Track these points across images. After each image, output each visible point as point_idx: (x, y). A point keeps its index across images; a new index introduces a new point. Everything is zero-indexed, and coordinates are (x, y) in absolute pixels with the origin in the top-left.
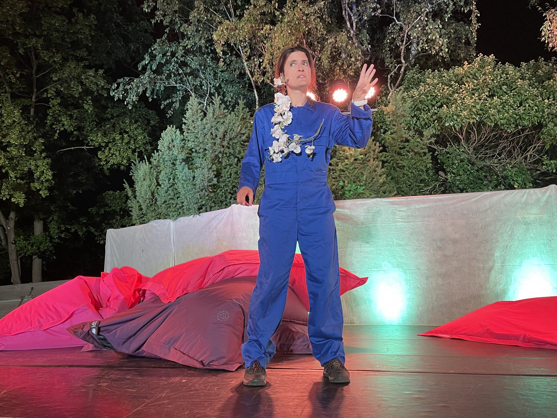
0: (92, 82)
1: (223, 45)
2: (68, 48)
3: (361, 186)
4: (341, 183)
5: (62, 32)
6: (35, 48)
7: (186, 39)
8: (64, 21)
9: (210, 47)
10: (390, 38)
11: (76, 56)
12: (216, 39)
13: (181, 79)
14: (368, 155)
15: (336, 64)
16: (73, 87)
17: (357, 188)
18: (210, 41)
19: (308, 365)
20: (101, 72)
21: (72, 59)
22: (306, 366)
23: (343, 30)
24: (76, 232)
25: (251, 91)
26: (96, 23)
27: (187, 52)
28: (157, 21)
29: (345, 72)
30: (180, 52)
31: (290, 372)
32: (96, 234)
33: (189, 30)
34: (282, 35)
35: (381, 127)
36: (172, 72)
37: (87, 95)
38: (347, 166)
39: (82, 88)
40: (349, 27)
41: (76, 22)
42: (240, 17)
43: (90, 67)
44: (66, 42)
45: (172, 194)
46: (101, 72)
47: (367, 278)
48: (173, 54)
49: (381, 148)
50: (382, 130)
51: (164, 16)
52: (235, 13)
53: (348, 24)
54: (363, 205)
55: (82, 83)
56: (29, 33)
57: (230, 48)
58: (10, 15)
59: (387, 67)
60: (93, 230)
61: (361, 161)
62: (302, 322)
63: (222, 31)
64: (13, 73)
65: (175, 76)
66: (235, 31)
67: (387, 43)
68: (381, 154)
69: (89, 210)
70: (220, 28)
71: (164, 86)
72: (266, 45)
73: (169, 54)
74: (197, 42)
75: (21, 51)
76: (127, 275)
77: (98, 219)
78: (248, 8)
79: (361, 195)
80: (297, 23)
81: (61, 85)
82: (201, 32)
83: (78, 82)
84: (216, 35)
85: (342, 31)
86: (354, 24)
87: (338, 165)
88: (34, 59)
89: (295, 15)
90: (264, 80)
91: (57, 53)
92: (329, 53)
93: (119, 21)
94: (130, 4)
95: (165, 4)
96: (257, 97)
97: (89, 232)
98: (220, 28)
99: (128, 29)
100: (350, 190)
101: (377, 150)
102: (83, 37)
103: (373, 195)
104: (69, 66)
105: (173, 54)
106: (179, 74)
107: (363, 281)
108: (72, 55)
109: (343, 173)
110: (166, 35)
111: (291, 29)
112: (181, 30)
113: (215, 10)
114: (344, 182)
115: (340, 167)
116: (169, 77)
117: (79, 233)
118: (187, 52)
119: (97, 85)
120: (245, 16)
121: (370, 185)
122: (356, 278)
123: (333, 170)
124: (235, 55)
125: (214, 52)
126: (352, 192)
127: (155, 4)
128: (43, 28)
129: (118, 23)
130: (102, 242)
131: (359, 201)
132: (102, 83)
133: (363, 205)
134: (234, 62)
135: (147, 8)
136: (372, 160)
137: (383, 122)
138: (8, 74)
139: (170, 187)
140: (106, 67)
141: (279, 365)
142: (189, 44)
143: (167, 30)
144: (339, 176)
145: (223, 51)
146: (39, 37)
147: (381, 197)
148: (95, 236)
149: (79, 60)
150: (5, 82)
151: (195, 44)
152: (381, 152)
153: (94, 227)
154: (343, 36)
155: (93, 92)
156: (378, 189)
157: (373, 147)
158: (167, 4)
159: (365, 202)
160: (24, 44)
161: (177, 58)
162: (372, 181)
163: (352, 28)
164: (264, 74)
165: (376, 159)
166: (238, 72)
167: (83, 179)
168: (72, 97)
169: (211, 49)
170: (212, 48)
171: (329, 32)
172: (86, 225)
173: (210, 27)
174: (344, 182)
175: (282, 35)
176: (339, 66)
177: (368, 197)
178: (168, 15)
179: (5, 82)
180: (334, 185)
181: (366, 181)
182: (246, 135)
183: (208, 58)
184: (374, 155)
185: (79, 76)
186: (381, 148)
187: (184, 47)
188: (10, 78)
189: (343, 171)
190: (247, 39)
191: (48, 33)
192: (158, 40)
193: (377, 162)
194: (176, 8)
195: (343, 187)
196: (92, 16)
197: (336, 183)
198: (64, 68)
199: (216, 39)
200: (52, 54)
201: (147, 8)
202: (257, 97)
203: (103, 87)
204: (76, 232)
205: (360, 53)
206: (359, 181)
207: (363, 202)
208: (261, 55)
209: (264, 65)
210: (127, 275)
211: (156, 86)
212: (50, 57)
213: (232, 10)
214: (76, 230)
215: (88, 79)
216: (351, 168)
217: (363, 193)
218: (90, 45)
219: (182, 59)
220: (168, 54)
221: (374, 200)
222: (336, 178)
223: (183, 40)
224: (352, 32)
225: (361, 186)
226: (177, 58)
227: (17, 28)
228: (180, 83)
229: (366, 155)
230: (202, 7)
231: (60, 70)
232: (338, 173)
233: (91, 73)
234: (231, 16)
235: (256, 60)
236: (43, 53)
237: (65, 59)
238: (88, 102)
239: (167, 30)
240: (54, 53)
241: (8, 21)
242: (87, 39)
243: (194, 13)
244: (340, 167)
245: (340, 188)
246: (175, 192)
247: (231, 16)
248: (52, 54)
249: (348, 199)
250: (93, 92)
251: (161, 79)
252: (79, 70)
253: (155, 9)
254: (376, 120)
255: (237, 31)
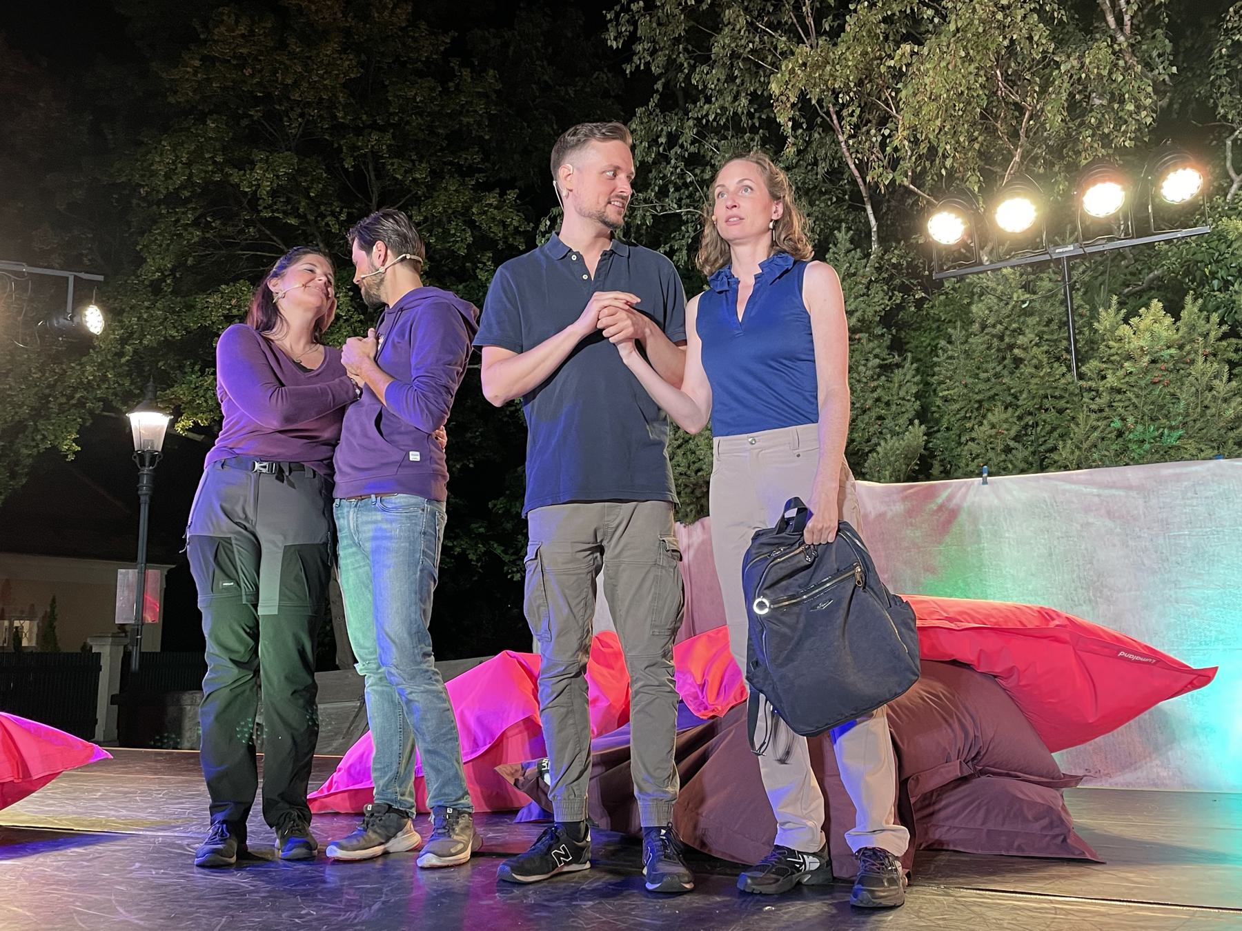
0: (494, 219)
1: (793, 105)
2: (442, 150)
3: (1171, 428)
4: (1117, 424)
5: (429, 114)
6: (375, 155)
7: (703, 100)
8: (432, 89)
9: (757, 115)
10: (1229, 42)
11: (459, 166)
12: (777, 92)
13: (690, 196)
14: (1188, 347)
15: (1082, 124)
16: (454, 235)
17: (1162, 434)
18: (762, 101)
19: (1075, 888)
20: (512, 195)
21: (449, 172)
22: (1075, 888)
23: (1098, 36)
24: (464, 554)
25: (856, 209)
26: (499, 86)
27: (704, 129)
28: (638, 67)
29: (1106, 140)
30: (690, 133)
31: (1031, 902)
32: (506, 558)
33: (712, 77)
34: (943, 64)
35: (1213, 275)
36: (671, 182)
37: (484, 250)
38: (1132, 379)
39: (473, 235)
40: (1113, 26)
41: (458, 89)
42: (835, 33)
43: (486, 187)
44: (438, 135)
45: (684, 462)
46: (512, 195)
47: (1216, 669)
48: (673, 139)
49: (1225, 328)
50: (1215, 282)
51: (653, 53)
52: (818, 23)
53: (1111, 20)
54: (1178, 478)
55: (471, 224)
56: (363, 122)
57: (807, 111)
58: (325, 88)
59: (1225, 117)
60: (498, 550)
61: (1171, 366)
62: (1036, 778)
63: (792, 71)
64: (333, 214)
65: (677, 189)
66: (822, 67)
67: (1221, 57)
68: (1224, 343)
69: (490, 506)
70: (787, 66)
71: (654, 216)
72: (903, 94)
73: (662, 140)
74: (727, 105)
75: (348, 164)
76: (610, 650)
77: (509, 526)
78: (855, 11)
79: (1172, 452)
80: (981, 30)
81: (430, 231)
82: (738, 81)
83: (465, 222)
84: (778, 82)
85: (1097, 40)
86: (1127, 18)
87: (1104, 377)
88: (373, 178)
89: (974, 10)
90: (893, 181)
91: (421, 162)
92: (1064, 96)
93: (546, 77)
94: (570, 35)
95: (654, 25)
96: (873, 222)
97: (489, 553)
98: (787, 66)
99: (567, 93)
100: (1143, 441)
101: (1213, 334)
102: (471, 120)
103: (1209, 452)
104: (446, 189)
105: (673, 139)
106: (686, 185)
107: (1203, 677)
108: (451, 163)
109: (1119, 397)
110: (656, 97)
111: (965, 48)
112: (694, 82)
113: (769, 25)
114: (1123, 419)
115: (1111, 380)
116: (663, 193)
117: (470, 557)
118: (704, 129)
119: (505, 226)
120: (848, 28)
121: (1198, 425)
122: (1183, 669)
123: (1090, 389)
124: (820, 126)
125: (772, 124)
126: (1147, 446)
127: (632, 28)
128: (391, 110)
129: (545, 82)
130: (517, 577)
131: (1168, 470)
132: (515, 220)
133: (1178, 478)
134: (814, 145)
135: (615, 39)
136: (1201, 359)
137: (1217, 261)
138: (323, 216)
139: (679, 447)
140: (520, 183)
141: (995, 882)
142: (711, 111)
143: (659, 86)
144: (1110, 406)
145: (792, 119)
146: (382, 129)
147: (1229, 457)
148: (504, 564)
149: (465, 172)
150: (317, 234)
151: (723, 108)
152: (1224, 337)
153: (500, 544)
154: (1097, 55)
155: (495, 242)
156: (1220, 436)
157: (1202, 327)
158: (659, 24)
159: (1185, 470)
160: (354, 148)
161: (682, 146)
162: (1202, 415)
163: (1122, 30)
164: (894, 164)
165: (1211, 358)
166: (822, 168)
167: (476, 437)
168: (452, 254)
169: (760, 118)
170: (764, 117)
171: (1060, 43)
172: (485, 539)
173: (759, 66)
174: (1123, 419)
175: (943, 64)
176: (1090, 126)
177: (1193, 457)
178: (661, 49)
179: (317, 234)
180: (1095, 428)
181: (1188, 415)
182: (858, 314)
183: (753, 140)
184: (1205, 347)
185: (467, 209)
186: (1225, 328)
187: (698, 120)
188: (327, 224)
189: (1119, 391)
190: (852, 85)
191: (401, 119)
192: (639, 111)
193: (1216, 365)
194: (681, 31)
195: (1120, 434)
196: (491, 72)
197: (1102, 424)
198: (436, 194)
199: (777, 92)
200: (409, 165)
201: (615, 39)
202: (873, 222)
203: (516, 228)
204: (464, 554)
205: (1150, 89)
206: (1166, 417)
207: (1178, 470)
208: (884, 120)
209: (896, 143)
210: (610, 650)
211: (635, 217)
212: (406, 172)
213: (810, 21)
214: (464, 551)
215: (485, 213)
216: (1143, 383)
217: (1178, 448)
218: (487, 137)
219: (693, 149)
220: (660, 140)
221: (1212, 464)
222: (1101, 410)
223: (695, 103)
224: (1121, 39)
225: (1171, 428)
226: (682, 146)
227: (340, 115)
228: (688, 206)
229: (1181, 347)
230: (742, 21)
231: (427, 198)
232: (1106, 398)
233: (492, 199)
234: (808, 34)
235: (873, 132)
236: (392, 164)
237: (436, 175)
238: (484, 264)
239: (659, 86)
240: (413, 161)
241: (321, 99)
242: (479, 124)
243: (723, 37)
244: (1111, 380)
245: (1113, 435)
246: (692, 458)
247: (808, 34)
248: (409, 165)
249: (1137, 463)
250: (495, 242)
251: (645, 201)
252: (466, 196)
253: (634, 38)
254: (1199, 257)
255: (828, 68)
